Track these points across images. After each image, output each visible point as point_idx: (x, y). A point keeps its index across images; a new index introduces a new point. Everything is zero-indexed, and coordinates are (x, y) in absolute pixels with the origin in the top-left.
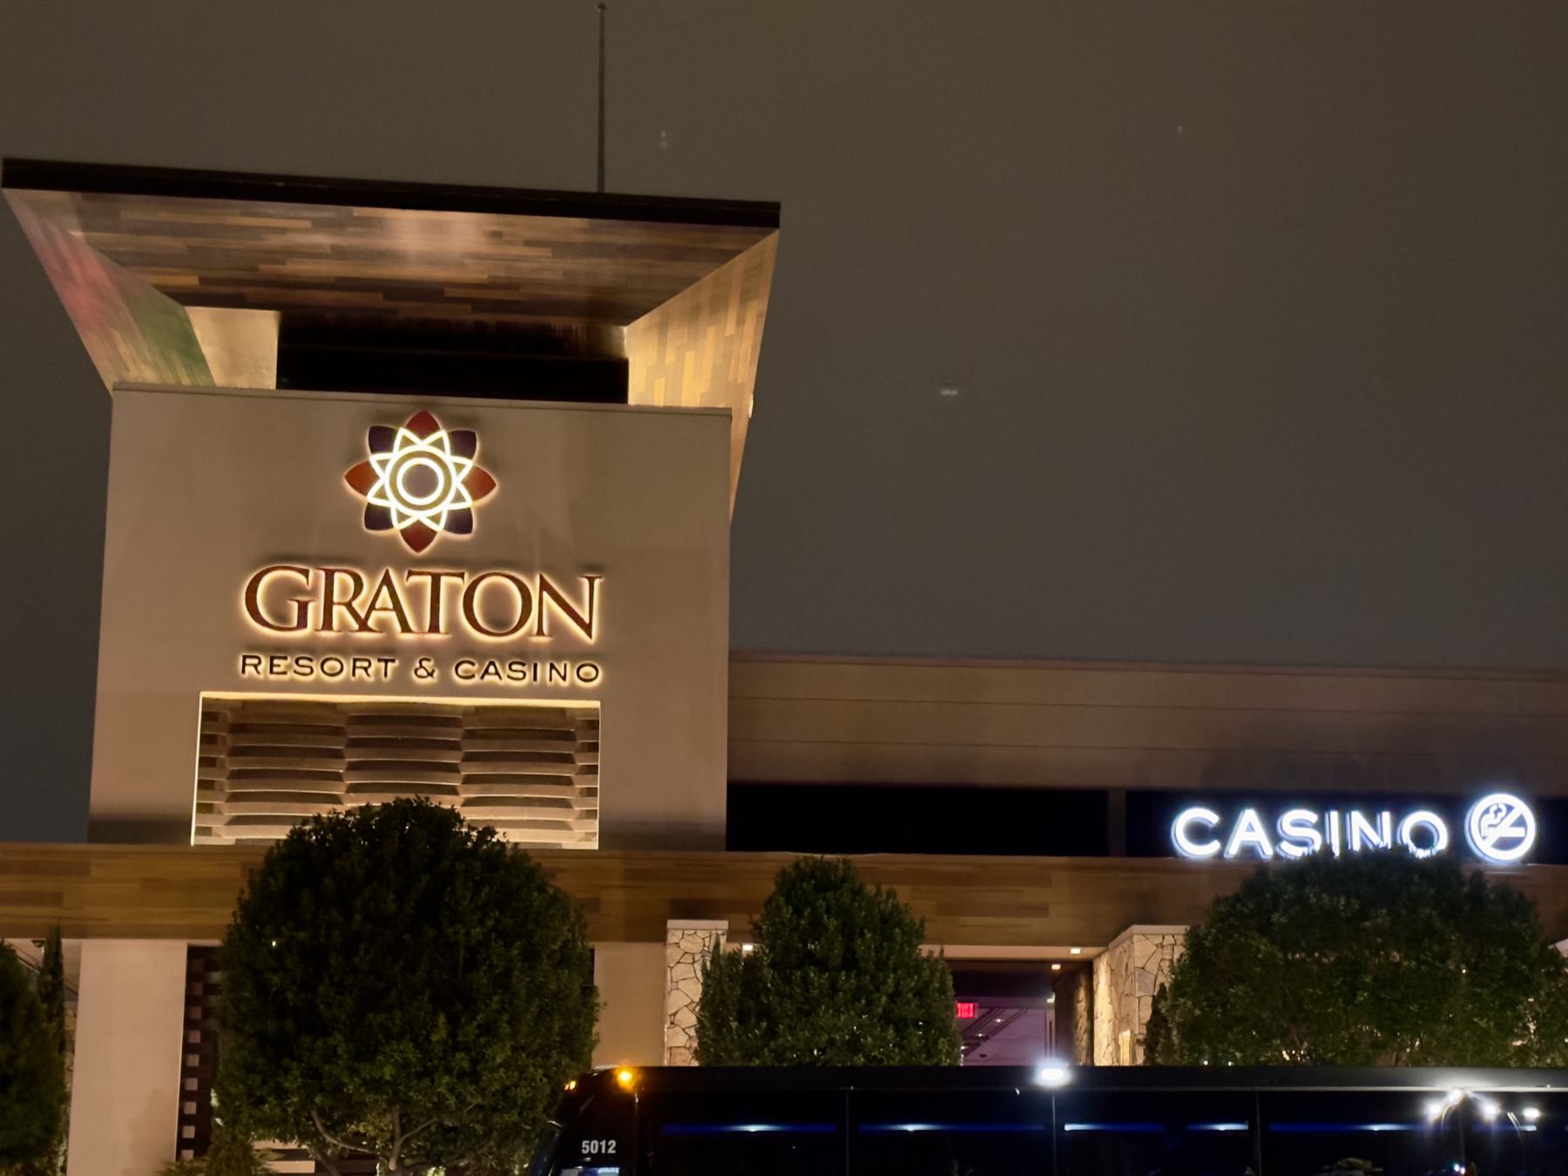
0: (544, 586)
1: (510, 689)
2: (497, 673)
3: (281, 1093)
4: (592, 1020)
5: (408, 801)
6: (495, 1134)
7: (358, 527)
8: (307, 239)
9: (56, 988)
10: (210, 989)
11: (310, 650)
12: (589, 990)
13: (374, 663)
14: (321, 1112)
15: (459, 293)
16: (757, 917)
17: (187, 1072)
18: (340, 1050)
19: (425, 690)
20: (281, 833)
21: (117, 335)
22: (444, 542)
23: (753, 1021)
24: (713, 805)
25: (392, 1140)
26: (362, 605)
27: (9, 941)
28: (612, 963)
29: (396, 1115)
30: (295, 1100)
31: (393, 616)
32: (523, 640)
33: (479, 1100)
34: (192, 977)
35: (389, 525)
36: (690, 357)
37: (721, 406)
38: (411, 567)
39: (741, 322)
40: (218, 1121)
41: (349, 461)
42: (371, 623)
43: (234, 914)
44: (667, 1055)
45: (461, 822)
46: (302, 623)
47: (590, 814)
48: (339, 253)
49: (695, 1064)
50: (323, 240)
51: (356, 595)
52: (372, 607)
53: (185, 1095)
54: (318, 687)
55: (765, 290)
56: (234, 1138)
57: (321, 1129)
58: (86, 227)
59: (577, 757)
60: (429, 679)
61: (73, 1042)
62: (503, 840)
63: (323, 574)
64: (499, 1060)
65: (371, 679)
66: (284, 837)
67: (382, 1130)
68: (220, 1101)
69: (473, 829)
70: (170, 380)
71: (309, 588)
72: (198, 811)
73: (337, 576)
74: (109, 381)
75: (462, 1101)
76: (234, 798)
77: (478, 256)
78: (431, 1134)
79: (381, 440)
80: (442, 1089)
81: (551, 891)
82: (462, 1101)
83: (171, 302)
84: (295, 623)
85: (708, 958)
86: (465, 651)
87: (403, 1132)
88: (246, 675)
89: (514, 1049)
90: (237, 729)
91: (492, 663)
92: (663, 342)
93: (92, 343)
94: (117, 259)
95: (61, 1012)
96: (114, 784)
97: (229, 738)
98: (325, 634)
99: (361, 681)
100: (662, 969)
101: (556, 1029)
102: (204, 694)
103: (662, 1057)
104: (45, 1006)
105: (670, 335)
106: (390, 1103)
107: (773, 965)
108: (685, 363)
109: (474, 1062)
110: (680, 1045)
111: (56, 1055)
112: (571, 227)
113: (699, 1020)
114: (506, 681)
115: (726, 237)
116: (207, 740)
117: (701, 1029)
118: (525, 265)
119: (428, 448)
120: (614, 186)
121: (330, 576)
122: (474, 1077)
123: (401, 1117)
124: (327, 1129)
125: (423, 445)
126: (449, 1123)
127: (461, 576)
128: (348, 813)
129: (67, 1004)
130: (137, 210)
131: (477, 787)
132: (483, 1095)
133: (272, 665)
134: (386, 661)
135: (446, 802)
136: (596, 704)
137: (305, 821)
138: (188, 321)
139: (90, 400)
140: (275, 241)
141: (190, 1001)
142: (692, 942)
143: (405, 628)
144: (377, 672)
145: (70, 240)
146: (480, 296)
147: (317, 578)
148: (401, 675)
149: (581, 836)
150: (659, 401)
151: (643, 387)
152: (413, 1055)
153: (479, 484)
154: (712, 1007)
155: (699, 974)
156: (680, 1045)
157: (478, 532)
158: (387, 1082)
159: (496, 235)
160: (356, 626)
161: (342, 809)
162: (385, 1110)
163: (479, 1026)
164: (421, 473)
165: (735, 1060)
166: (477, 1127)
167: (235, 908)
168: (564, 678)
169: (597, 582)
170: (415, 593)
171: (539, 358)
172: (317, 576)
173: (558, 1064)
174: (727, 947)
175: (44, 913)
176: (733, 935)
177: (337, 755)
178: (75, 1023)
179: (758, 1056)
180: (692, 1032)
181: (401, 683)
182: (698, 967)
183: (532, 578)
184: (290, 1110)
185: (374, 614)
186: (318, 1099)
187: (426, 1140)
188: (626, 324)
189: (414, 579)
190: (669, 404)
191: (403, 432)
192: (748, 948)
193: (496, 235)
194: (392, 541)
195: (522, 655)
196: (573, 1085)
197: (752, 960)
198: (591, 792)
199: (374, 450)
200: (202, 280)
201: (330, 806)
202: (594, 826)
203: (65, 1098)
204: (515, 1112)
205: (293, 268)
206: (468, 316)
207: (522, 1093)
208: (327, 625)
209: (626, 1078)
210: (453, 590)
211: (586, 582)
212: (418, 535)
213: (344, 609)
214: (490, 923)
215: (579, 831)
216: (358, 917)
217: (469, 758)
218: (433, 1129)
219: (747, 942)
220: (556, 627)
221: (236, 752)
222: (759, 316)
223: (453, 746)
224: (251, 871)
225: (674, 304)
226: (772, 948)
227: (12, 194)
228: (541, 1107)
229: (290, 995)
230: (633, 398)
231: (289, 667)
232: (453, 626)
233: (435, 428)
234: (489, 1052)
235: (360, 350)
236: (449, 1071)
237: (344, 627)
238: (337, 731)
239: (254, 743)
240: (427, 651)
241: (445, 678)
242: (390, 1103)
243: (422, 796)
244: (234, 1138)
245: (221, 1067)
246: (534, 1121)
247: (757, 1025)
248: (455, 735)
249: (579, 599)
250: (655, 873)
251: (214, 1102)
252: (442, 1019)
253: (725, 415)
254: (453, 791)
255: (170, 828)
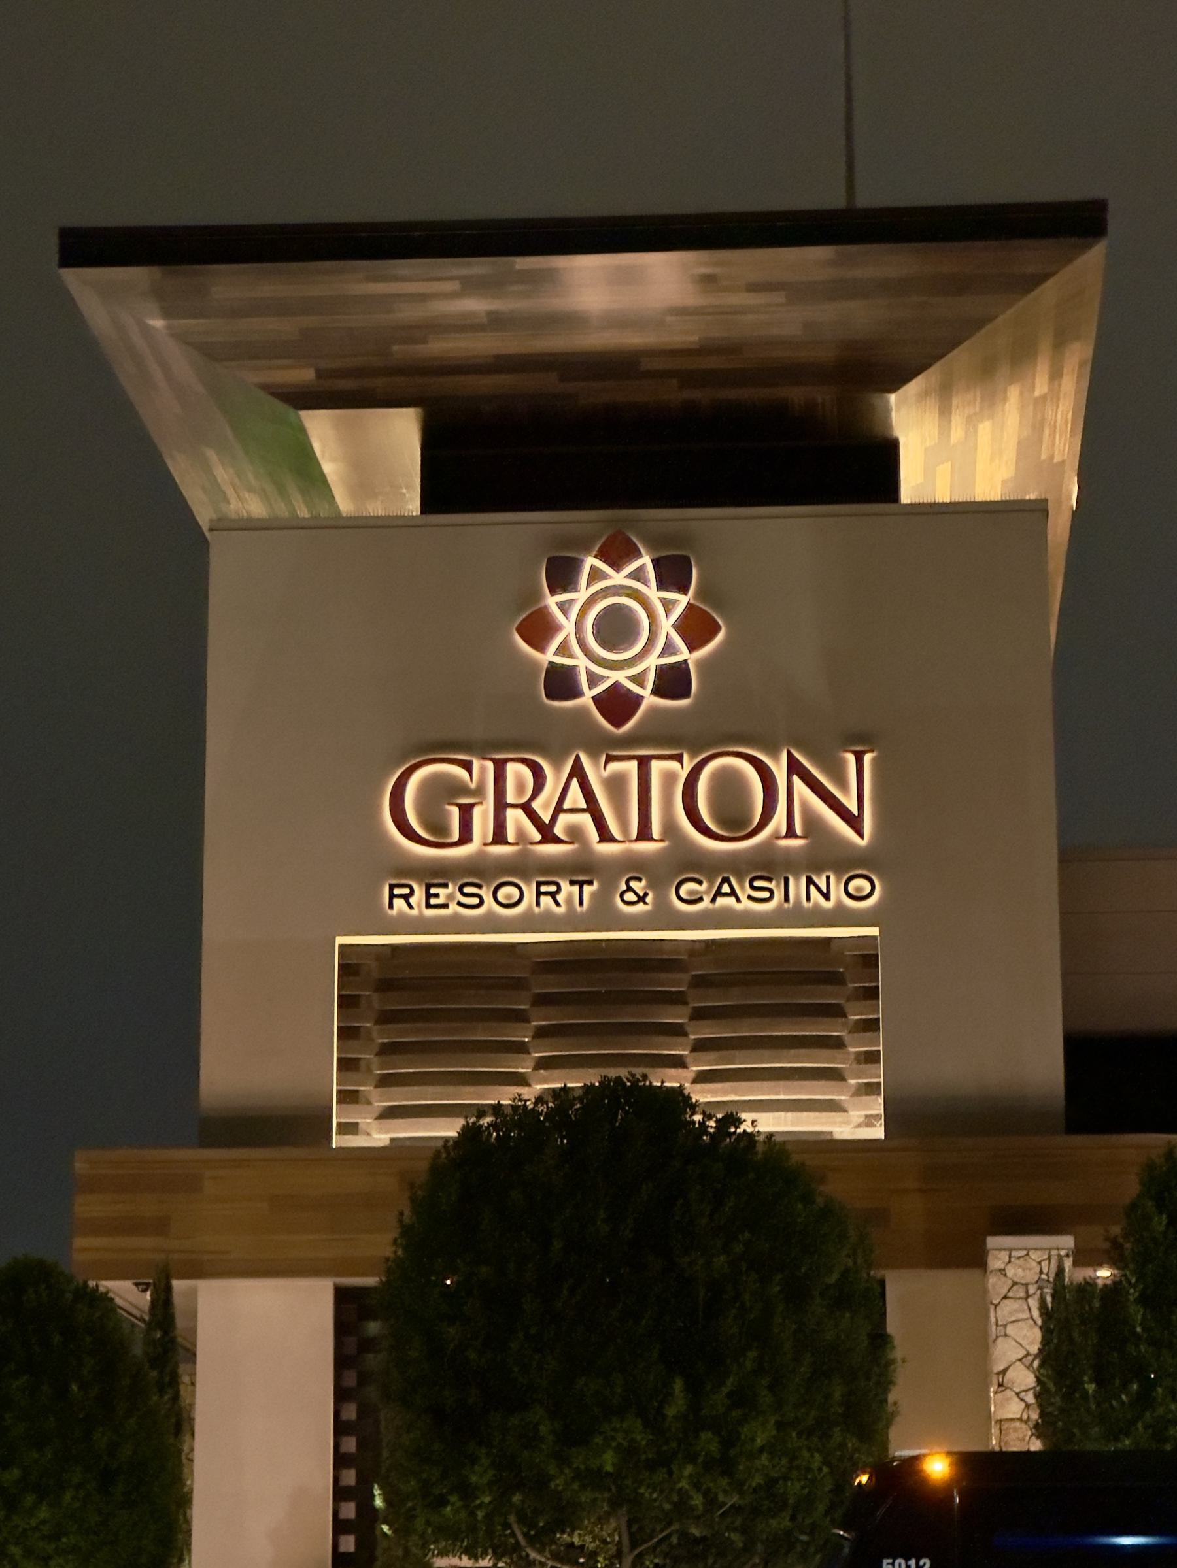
0: (794, 767)
1: (752, 915)
2: (733, 893)
3: (467, 1492)
4: (885, 1383)
5: (618, 1079)
6: (760, 1547)
7: (536, 697)
8: (453, 306)
9: (167, 1348)
10: (367, 1345)
11: (476, 873)
12: (880, 1339)
13: (565, 886)
14: (522, 1519)
15: (658, 365)
16: (1116, 1230)
17: (341, 1461)
18: (543, 1429)
19: (634, 920)
20: (449, 1129)
21: (212, 455)
22: (654, 711)
23: (1117, 1382)
24: (1042, 1067)
25: (619, 1555)
26: (546, 806)
27: (105, 1285)
28: (911, 1299)
29: (623, 1522)
30: (487, 1500)
31: (586, 820)
32: (768, 845)
33: (734, 1499)
34: (343, 1328)
35: (576, 693)
36: (985, 428)
37: (1032, 496)
38: (607, 749)
39: (1056, 375)
40: (385, 1528)
41: (521, 609)
42: (558, 830)
43: (395, 1241)
44: (994, 1431)
45: (694, 1107)
46: (466, 837)
47: (871, 1089)
48: (496, 322)
49: (1036, 1446)
50: (476, 305)
51: (534, 796)
52: (559, 809)
53: (340, 1493)
54: (492, 924)
55: (1091, 331)
56: (407, 1551)
57: (523, 1542)
58: (167, 314)
59: (849, 1007)
60: (641, 907)
61: (191, 1420)
62: (749, 1130)
63: (490, 765)
64: (759, 1442)
65: (561, 910)
66: (453, 1134)
67: (604, 1542)
68: (386, 1500)
69: (710, 1117)
70: (282, 510)
71: (473, 786)
72: (339, 1133)
73: (511, 768)
74: (204, 516)
75: (711, 1502)
76: (385, 1082)
77: (682, 312)
78: (671, 1546)
79: (562, 576)
80: (684, 1484)
81: (820, 1201)
82: (711, 1502)
83: (281, 407)
84: (456, 836)
85: (1048, 1290)
86: (686, 864)
87: (633, 1546)
88: (394, 912)
89: (780, 1426)
90: (385, 986)
91: (726, 880)
92: (945, 412)
93: (181, 469)
94: (210, 353)
95: (174, 1381)
96: (233, 1064)
97: (376, 997)
98: (786, 905)
99: (548, 914)
100: (982, 1306)
101: (837, 1395)
102: (341, 940)
103: (989, 1439)
104: (154, 1374)
105: (955, 401)
106: (615, 1504)
107: (1143, 1300)
108: (973, 444)
109: (728, 1443)
110: (1012, 1418)
111: (171, 1440)
112: (810, 261)
113: (1039, 1381)
114: (746, 904)
115: (1028, 255)
116: (346, 1002)
117: (1042, 1395)
118: (750, 317)
119: (633, 582)
120: (866, 199)
121: (500, 766)
122: (724, 1465)
123: (630, 1524)
124: (532, 1541)
125: (618, 578)
126: (696, 1531)
127: (679, 758)
128: (539, 1100)
129: (182, 1368)
130: (230, 284)
131: (712, 1055)
132: (741, 1493)
133: (429, 896)
134: (581, 884)
135: (672, 1079)
136: (874, 931)
137: (481, 1112)
138: (303, 431)
139: (179, 548)
140: (409, 313)
141: (341, 1362)
142: (1023, 1269)
143: (605, 835)
144: (569, 900)
145: (146, 331)
146: (690, 367)
147: (483, 770)
148: (602, 898)
149: (858, 1121)
150: (943, 494)
151: (919, 479)
152: (641, 1437)
153: (695, 628)
154: (1057, 1361)
155: (1036, 1313)
156: (1012, 1418)
157: (696, 696)
158: (608, 1474)
159: (708, 281)
160: (538, 837)
161: (529, 1093)
162: (608, 1514)
163: (730, 1395)
164: (617, 615)
165: (1093, 1442)
166: (735, 1536)
167: (395, 1233)
168: (827, 896)
169: (868, 758)
170: (616, 785)
171: (778, 445)
172: (484, 768)
173: (842, 1446)
174: (1075, 1275)
175: (145, 1245)
176: (1083, 1257)
177: (520, 1017)
178: (193, 1394)
179: (1127, 1435)
180: (1030, 1398)
181: (603, 915)
182: (1034, 1303)
183: (775, 756)
184: (480, 1514)
185: (563, 819)
186: (517, 1498)
187: (666, 1555)
188: (894, 390)
189: (614, 766)
190: (958, 498)
191: (590, 561)
192: (1104, 1273)
193: (708, 281)
194: (583, 712)
195: (766, 867)
196: (864, 1479)
197: (1113, 1291)
198: (871, 1058)
199: (553, 592)
200: (320, 374)
201: (515, 1090)
202: (877, 1105)
203: (185, 1501)
204: (786, 1515)
205: (439, 347)
206: (673, 395)
207: (794, 1488)
208: (500, 837)
209: (938, 1467)
210: (669, 778)
211: (851, 758)
212: (617, 704)
213: (520, 813)
214: (738, 1248)
215: (856, 1114)
216: (557, 1245)
217: (699, 1015)
218: (674, 1540)
219: (1100, 1265)
220: (813, 824)
221: (386, 1018)
222: (1081, 365)
223: (677, 999)
224: (412, 1185)
225: (960, 357)
226: (1141, 1277)
227: (72, 278)
228: (821, 1508)
229: (472, 1355)
230: (908, 494)
231: (450, 897)
232: (670, 829)
233: (635, 554)
234: (745, 1431)
235: (535, 453)
236: (692, 1458)
237: (522, 836)
238: (518, 984)
239: (413, 1004)
240: (635, 867)
241: (662, 904)
242: (615, 1504)
243: (638, 1071)
244: (407, 1551)
245: (385, 1453)
246: (813, 1529)
247: (1125, 1385)
248: (677, 983)
249: (842, 783)
250: (965, 1169)
251: (379, 1502)
252: (678, 1385)
253: (1039, 510)
254: (678, 1063)
255: (301, 1126)
